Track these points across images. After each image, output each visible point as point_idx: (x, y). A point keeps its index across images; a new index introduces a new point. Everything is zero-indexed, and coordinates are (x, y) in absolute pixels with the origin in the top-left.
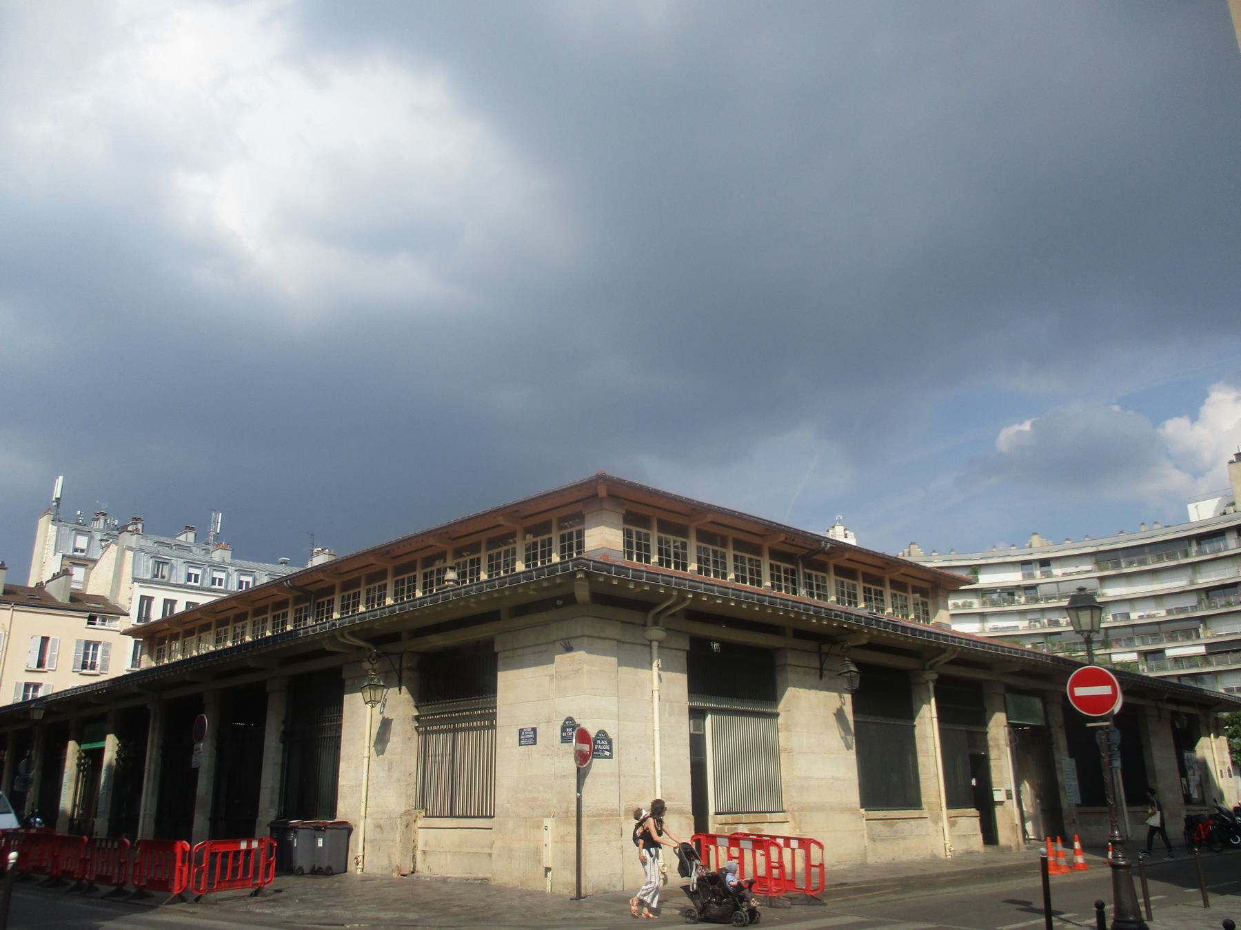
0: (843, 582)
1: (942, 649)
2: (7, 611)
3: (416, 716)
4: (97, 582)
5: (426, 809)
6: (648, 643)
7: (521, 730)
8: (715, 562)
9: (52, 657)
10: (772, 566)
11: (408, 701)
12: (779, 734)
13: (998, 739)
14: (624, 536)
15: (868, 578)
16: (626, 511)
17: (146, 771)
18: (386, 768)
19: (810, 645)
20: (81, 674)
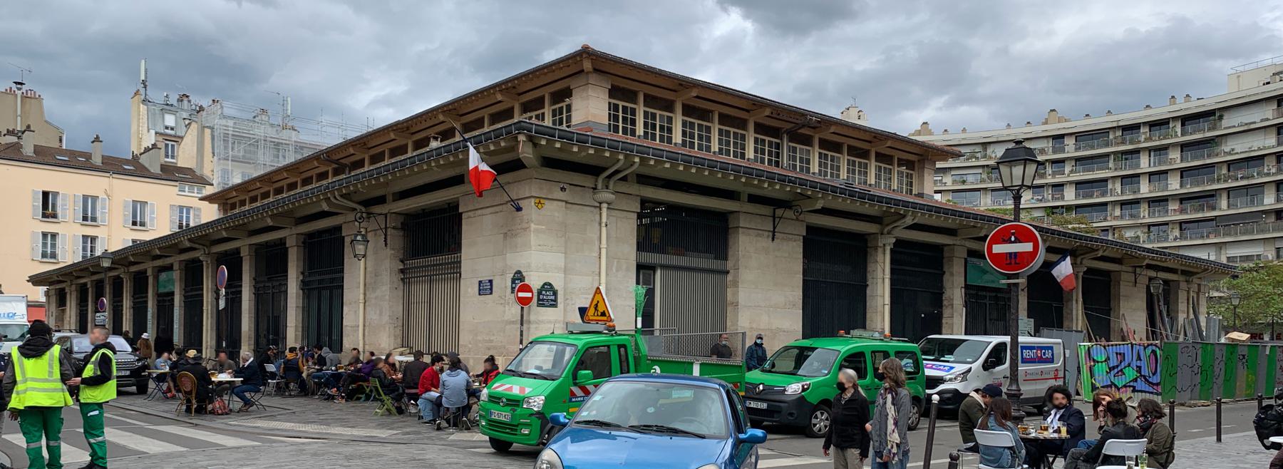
2: (175, 188)
3: (401, 269)
4: (185, 157)
6: (598, 205)
7: (480, 282)
8: (700, 138)
10: (756, 140)
12: (728, 289)
13: (953, 299)
15: (853, 151)
16: (612, 86)
17: (205, 311)
18: (378, 312)
19: (767, 210)
20: (82, 225)
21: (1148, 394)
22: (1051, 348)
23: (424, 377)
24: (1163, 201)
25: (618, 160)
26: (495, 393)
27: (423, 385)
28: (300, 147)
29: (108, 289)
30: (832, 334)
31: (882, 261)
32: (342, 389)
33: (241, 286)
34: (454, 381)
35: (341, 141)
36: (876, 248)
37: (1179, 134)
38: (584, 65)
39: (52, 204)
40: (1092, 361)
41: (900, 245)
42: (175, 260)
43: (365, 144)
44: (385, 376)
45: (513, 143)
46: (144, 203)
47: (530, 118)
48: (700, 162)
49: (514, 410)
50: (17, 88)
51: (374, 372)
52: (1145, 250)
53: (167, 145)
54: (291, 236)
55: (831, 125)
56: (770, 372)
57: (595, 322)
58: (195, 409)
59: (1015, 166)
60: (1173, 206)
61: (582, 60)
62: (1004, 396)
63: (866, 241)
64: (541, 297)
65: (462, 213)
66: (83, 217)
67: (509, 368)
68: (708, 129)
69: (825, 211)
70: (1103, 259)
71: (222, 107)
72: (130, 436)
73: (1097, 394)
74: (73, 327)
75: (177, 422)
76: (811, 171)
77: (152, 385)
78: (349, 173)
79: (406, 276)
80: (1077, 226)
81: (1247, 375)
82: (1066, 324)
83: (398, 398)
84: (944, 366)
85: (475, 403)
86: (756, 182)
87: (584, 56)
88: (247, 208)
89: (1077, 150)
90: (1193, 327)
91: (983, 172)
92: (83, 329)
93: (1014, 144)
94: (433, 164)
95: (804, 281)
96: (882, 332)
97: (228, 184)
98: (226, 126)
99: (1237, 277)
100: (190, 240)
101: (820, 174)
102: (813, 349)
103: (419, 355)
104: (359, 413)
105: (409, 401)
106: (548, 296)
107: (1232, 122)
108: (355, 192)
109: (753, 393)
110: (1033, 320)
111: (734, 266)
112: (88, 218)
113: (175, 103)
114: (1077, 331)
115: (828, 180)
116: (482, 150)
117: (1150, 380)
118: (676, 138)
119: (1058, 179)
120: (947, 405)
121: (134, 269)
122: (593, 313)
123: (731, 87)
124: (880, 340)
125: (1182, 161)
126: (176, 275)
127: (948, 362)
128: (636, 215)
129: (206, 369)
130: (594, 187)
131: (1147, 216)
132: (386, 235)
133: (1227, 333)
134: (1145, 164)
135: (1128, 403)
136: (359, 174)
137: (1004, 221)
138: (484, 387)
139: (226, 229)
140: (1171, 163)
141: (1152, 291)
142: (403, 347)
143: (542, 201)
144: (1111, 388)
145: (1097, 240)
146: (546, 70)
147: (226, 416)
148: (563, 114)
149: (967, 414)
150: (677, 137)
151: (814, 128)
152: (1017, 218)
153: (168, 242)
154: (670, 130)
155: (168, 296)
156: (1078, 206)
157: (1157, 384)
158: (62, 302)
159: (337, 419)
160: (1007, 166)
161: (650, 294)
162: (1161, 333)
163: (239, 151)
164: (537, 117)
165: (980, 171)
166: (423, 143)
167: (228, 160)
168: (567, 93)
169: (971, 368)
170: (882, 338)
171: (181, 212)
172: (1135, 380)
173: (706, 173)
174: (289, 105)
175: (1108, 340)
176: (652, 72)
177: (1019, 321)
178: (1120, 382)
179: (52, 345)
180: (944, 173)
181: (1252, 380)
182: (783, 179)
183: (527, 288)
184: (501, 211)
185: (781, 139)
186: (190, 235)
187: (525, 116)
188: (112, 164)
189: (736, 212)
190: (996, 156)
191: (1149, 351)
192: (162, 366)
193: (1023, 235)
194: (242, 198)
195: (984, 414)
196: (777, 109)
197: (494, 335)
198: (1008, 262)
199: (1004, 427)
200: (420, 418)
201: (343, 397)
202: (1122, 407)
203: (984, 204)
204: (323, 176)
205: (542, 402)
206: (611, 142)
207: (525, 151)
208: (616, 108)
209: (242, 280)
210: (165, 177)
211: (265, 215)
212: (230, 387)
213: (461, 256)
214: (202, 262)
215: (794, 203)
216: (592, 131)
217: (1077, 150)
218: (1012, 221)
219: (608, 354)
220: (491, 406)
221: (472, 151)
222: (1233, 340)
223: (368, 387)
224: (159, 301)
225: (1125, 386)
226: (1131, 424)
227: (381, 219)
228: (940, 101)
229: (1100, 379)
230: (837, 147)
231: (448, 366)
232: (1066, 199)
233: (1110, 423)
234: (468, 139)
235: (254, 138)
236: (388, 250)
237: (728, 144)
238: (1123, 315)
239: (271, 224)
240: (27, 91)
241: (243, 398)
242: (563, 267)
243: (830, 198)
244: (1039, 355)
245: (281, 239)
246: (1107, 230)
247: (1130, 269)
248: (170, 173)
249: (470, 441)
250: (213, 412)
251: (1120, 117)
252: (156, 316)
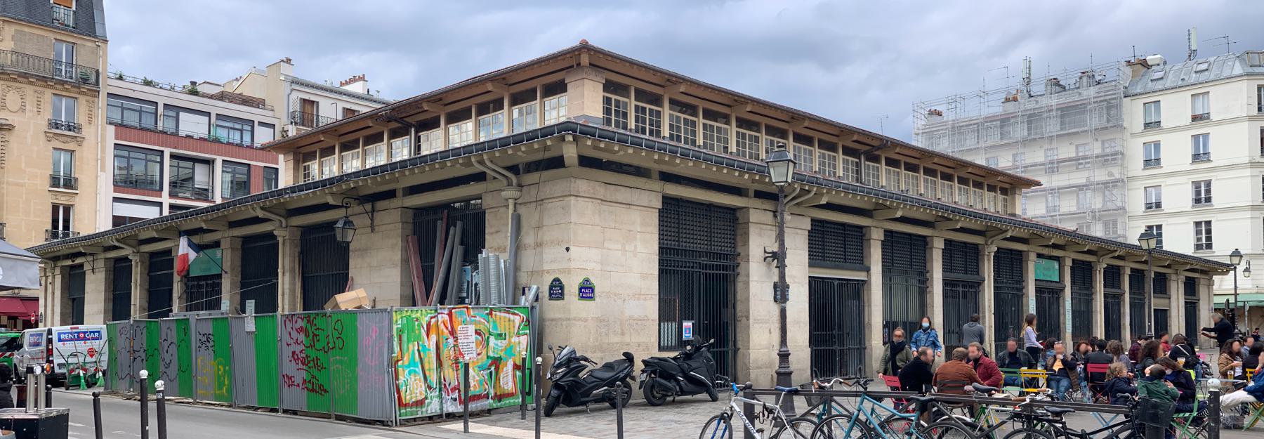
0: (799, 148)
14: (604, 104)
16: (606, 80)
54: (284, 235)
61: (580, 54)
70: (1013, 239)
206: (683, 150)
214: (131, 260)
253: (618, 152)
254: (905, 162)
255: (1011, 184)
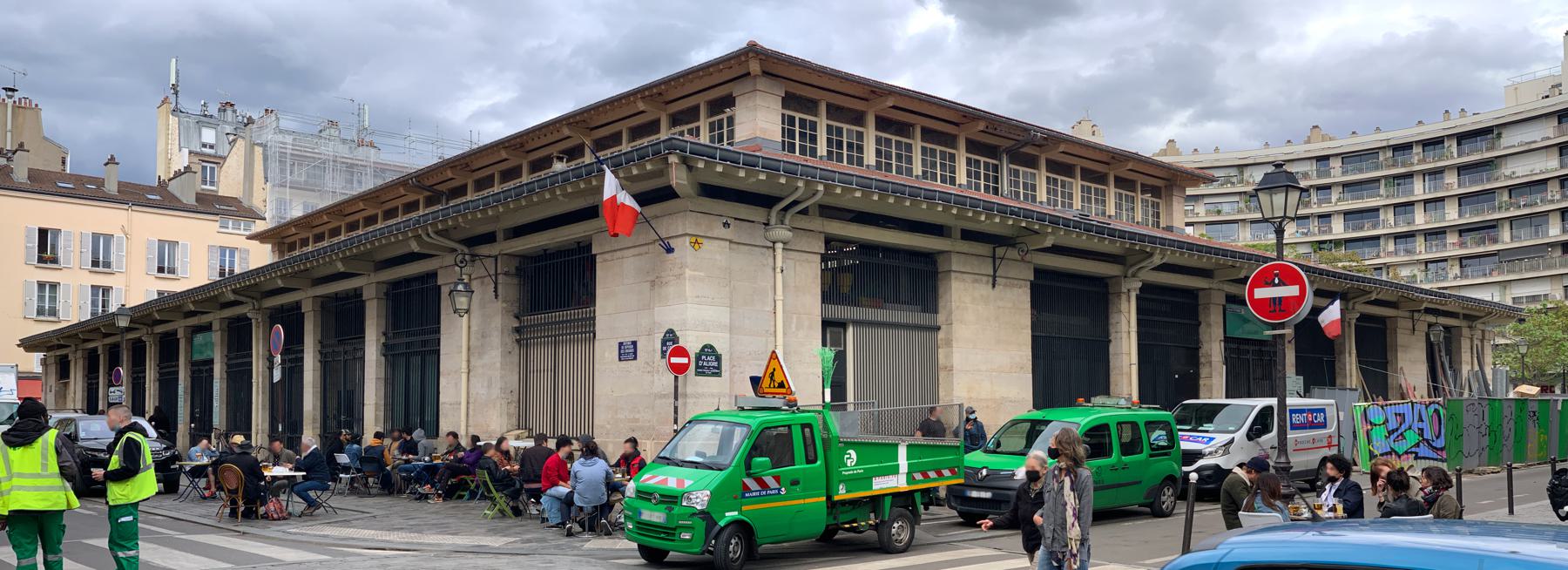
1: (1147, 252)
4: (228, 183)
5: (529, 430)
6: (771, 245)
7: (621, 344)
8: (899, 157)
9: (120, 257)
10: (969, 162)
11: (506, 311)
15: (1088, 175)
16: (786, 93)
17: (254, 384)
18: (486, 384)
19: (983, 249)
21: (1431, 461)
22: (1323, 411)
23: (547, 467)
24: (1436, 233)
25: (797, 188)
26: (648, 487)
27: (548, 478)
28: (380, 169)
29: (125, 357)
30: (1069, 403)
31: (1127, 310)
32: (438, 486)
33: (303, 351)
34: (589, 472)
35: (436, 161)
36: (1119, 294)
37: (1455, 155)
38: (750, 66)
39: (51, 245)
40: (1368, 424)
41: (1147, 290)
42: (216, 318)
43: (467, 165)
44: (497, 466)
45: (661, 166)
46: (174, 244)
47: (682, 133)
48: (899, 191)
49: (670, 509)
50: (7, 95)
51: (481, 461)
52: (1422, 291)
53: (204, 168)
54: (369, 285)
55: (1060, 142)
56: (994, 452)
57: (771, 396)
58: (242, 512)
59: (1275, 194)
60: (1452, 239)
61: (747, 61)
62: (1272, 471)
63: (1106, 286)
64: (700, 363)
65: (595, 255)
66: (92, 261)
67: (661, 455)
68: (909, 148)
69: (1056, 250)
71: (278, 119)
72: (155, 549)
73: (1375, 464)
74: (79, 406)
75: (218, 529)
76: (1038, 200)
77: (184, 481)
78: (447, 204)
79: (523, 336)
80: (1348, 264)
81: (1539, 435)
82: (1338, 382)
83: (515, 496)
84: (1203, 437)
85: (620, 500)
86: (970, 214)
87: (751, 55)
88: (310, 248)
89: (1344, 173)
90: (1478, 381)
91: (1241, 200)
92: (92, 408)
93: (1274, 168)
94: (558, 193)
95: (1034, 338)
96: (1129, 399)
97: (285, 218)
98: (282, 143)
99: (1524, 320)
100: (234, 292)
101: (1049, 204)
102: (1047, 422)
103: (541, 438)
104: (460, 516)
105: (529, 499)
106: (709, 362)
107: (1512, 140)
108: (455, 228)
109: (975, 480)
110: (1302, 377)
111: (947, 320)
112: (98, 263)
113: (216, 114)
114: (1351, 389)
115: (1058, 211)
116: (621, 175)
117: (1434, 444)
118: (868, 159)
119: (1325, 209)
120: (1208, 484)
121: (160, 329)
122: (769, 383)
123: (935, 95)
124: (1127, 408)
125: (1459, 186)
126: (216, 337)
127: (1207, 431)
128: (819, 256)
129: (257, 460)
130: (766, 222)
131: (1423, 252)
132: (496, 284)
133: (1515, 386)
134: (1419, 190)
135: (1410, 473)
136: (459, 205)
137: (1266, 260)
138: (629, 480)
139: (282, 277)
140: (1447, 190)
141: (1432, 339)
142: (519, 429)
143: (699, 240)
144: (1391, 455)
145: (1369, 281)
146: (701, 73)
147: (282, 522)
148: (725, 129)
149: (1230, 496)
150: (870, 157)
151: (1039, 146)
152: (1280, 256)
153: (205, 294)
154: (860, 149)
155: (207, 365)
156: (1348, 241)
157: (1442, 449)
158: (63, 372)
159: (433, 525)
160: (1266, 193)
161: (840, 358)
162: (1444, 389)
163: (300, 176)
164: (690, 132)
165: (1236, 198)
166: (545, 163)
167: (286, 186)
168: (729, 101)
169: (1233, 438)
170: (1130, 406)
171: (223, 254)
172: (1417, 445)
173: (908, 204)
174: (367, 115)
175: (1386, 399)
176: (836, 76)
177: (1287, 379)
178: (1401, 447)
179: (47, 428)
180: (1195, 201)
181: (1544, 440)
182: (1003, 210)
183: (681, 352)
184: (646, 253)
185: (1000, 160)
186: (235, 285)
187: (674, 130)
188: (132, 193)
189: (947, 252)
190: (1254, 181)
191: (1431, 410)
192: (198, 456)
193: (1289, 276)
194: (303, 235)
195: (1249, 493)
196: (994, 123)
197: (639, 412)
198: (1272, 309)
199: (1272, 507)
200: (544, 520)
201: (439, 496)
202: (1404, 478)
203: (1243, 239)
204: (412, 207)
205: (706, 498)
206: (788, 165)
207: (678, 177)
208: (791, 120)
209: (303, 343)
210: (202, 209)
211: (334, 258)
212: (289, 484)
213: (594, 310)
215: (1019, 240)
216: (760, 150)
217: (1344, 173)
218: (1275, 260)
219: (789, 435)
220: (640, 504)
221: (609, 177)
222: (1523, 394)
223: (472, 481)
224: (193, 372)
225: (1406, 453)
226: (1414, 498)
227: (490, 263)
228: (1184, 115)
229: (1378, 445)
230: (1067, 170)
231: (580, 453)
232: (1334, 232)
233: (1390, 498)
234: (603, 160)
235: (319, 159)
236: (500, 303)
237: (934, 165)
238: (1401, 368)
239: (342, 270)
240: (20, 99)
241: (306, 499)
242: (728, 325)
243: (1062, 233)
244: (1310, 419)
245: (355, 289)
246: (1381, 268)
247: (1408, 314)
248: (209, 205)
249: (612, 550)
250: (266, 517)
251: (1390, 135)
252: (189, 391)
253: (983, 222)
254: (1082, 169)
255: (1168, 180)
